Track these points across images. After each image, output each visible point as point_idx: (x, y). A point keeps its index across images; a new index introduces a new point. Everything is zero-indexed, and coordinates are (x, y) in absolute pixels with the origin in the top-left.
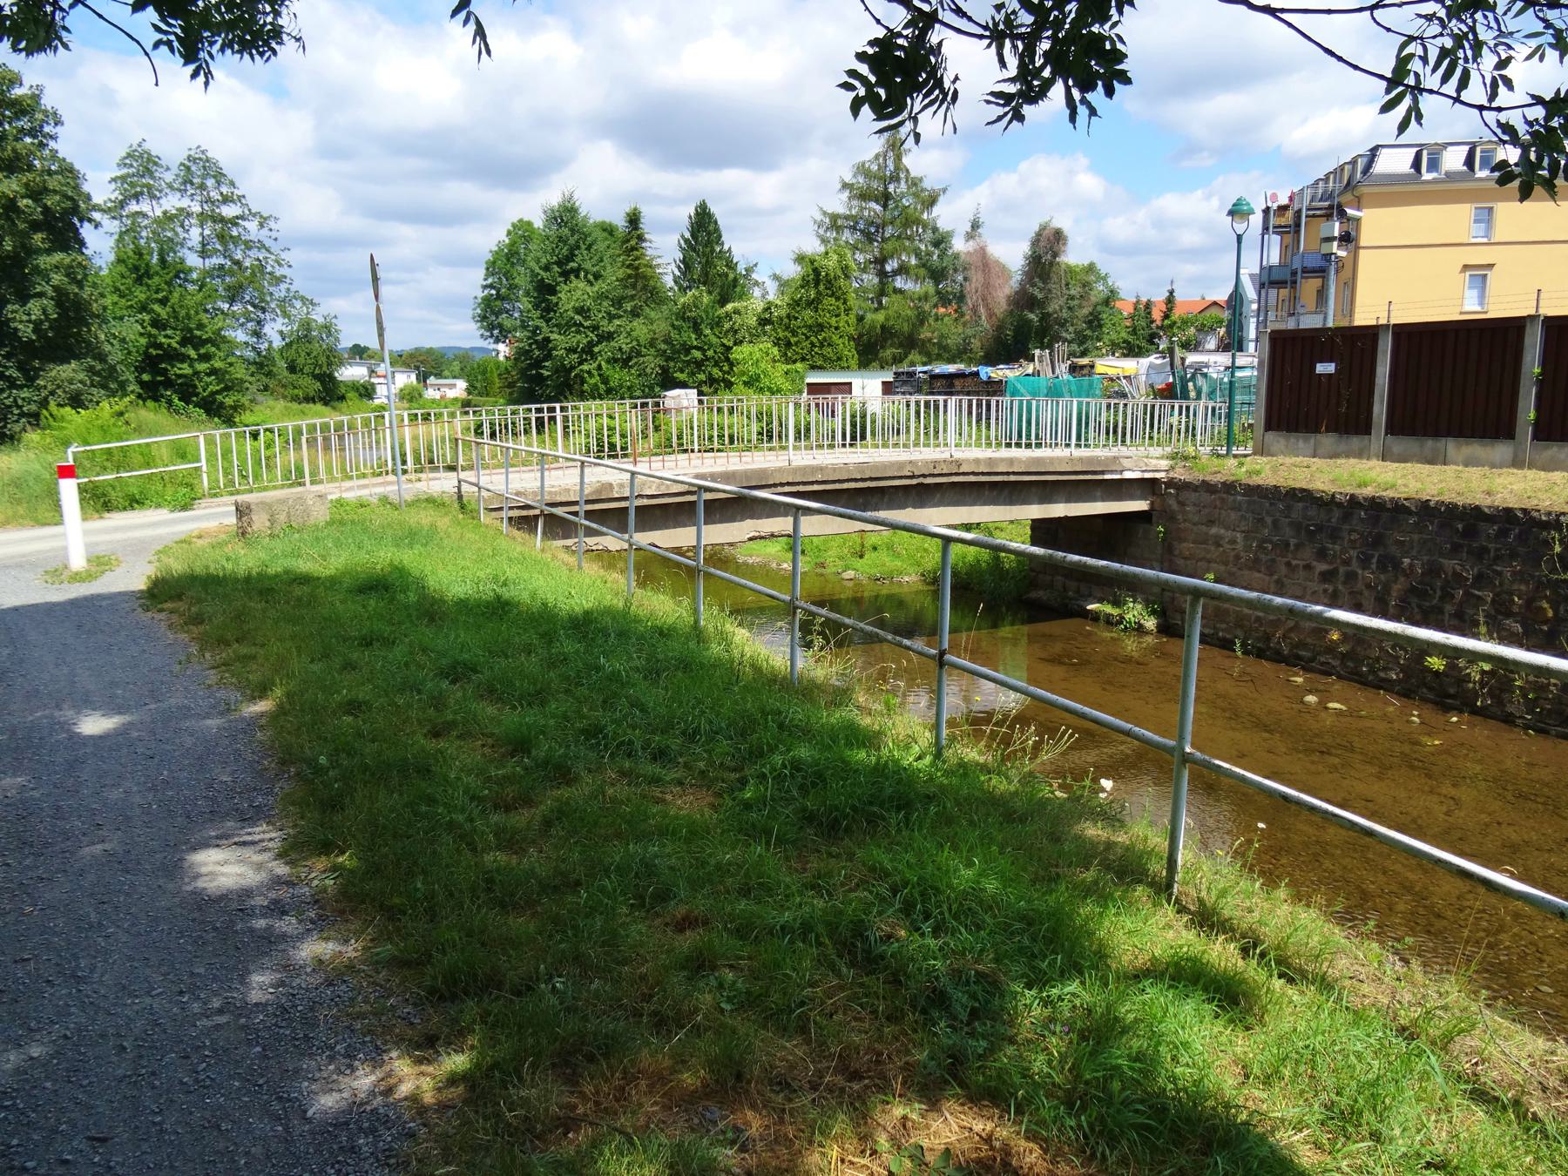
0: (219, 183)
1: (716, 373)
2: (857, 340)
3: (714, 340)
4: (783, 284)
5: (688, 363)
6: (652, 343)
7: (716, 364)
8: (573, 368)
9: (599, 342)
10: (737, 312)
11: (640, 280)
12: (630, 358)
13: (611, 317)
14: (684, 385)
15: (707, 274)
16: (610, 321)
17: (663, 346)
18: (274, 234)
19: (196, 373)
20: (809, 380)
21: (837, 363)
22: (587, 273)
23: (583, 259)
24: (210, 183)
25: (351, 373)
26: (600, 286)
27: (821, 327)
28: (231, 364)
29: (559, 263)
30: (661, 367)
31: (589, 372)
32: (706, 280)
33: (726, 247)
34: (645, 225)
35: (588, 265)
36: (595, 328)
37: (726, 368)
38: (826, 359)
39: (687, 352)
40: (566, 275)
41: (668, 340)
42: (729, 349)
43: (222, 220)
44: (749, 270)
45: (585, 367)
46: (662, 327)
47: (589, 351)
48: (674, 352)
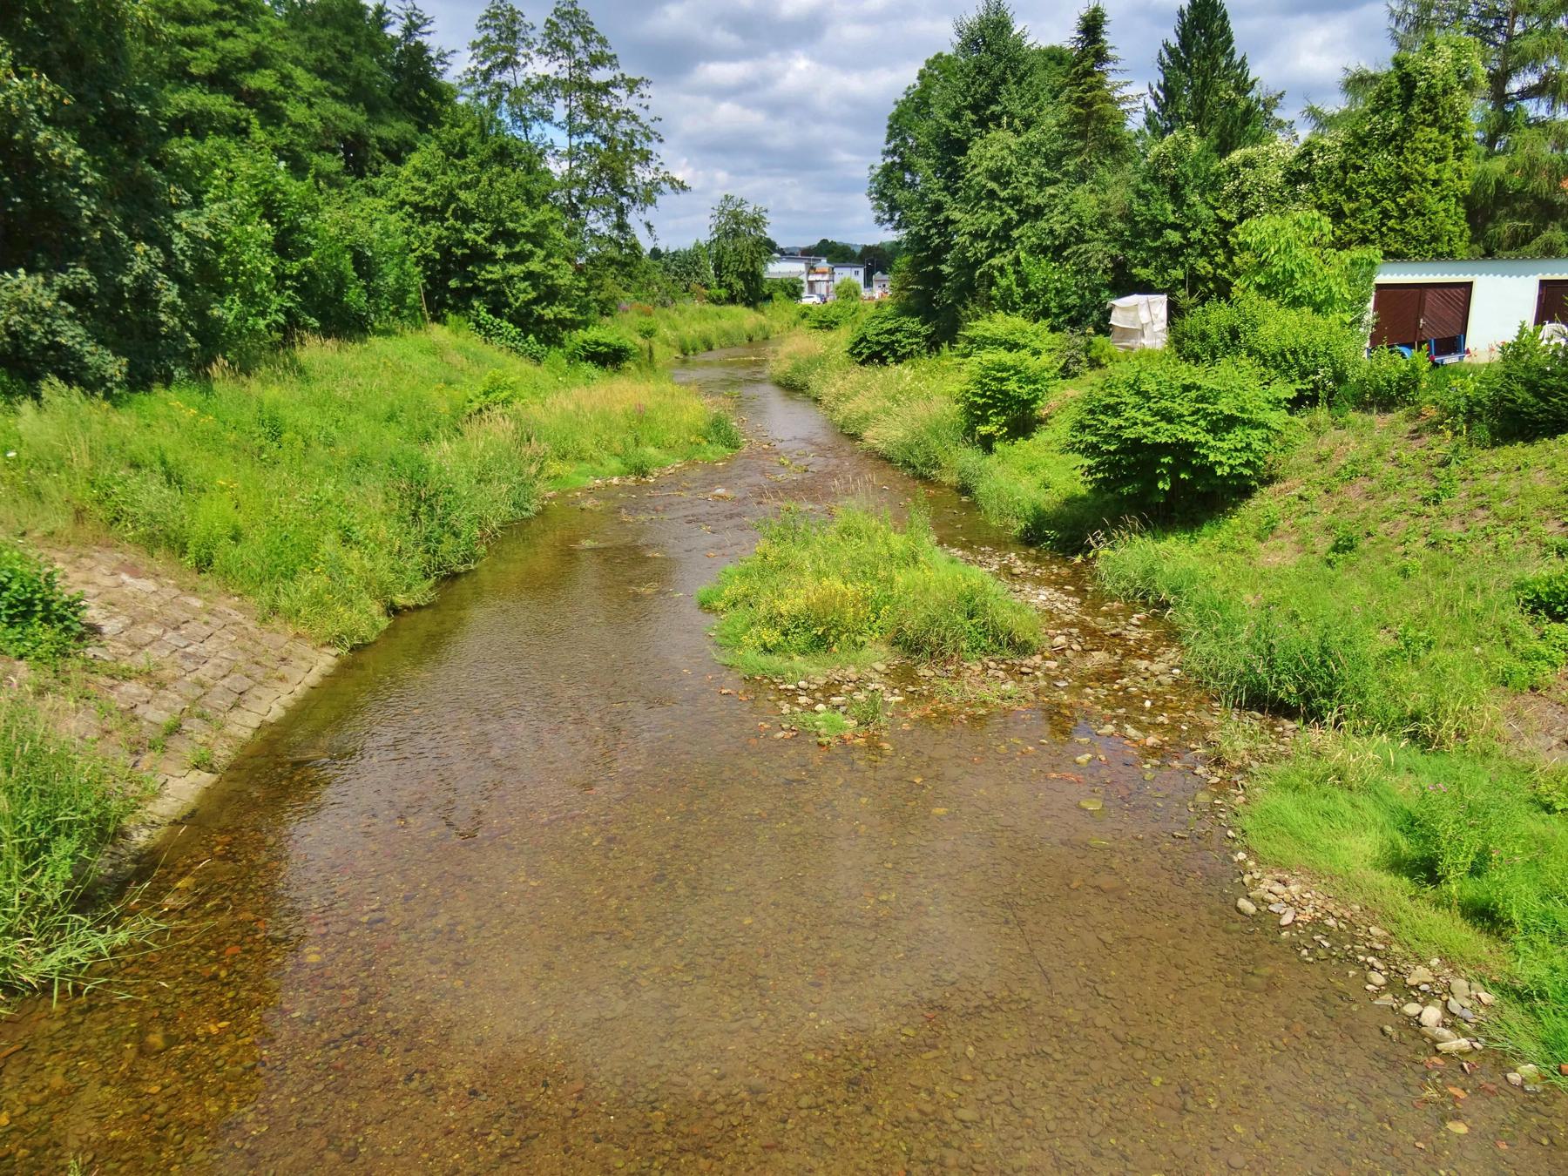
0: (587, 41)
1: (1203, 267)
2: (1467, 201)
3: (1204, 212)
4: (1324, 122)
5: (1156, 252)
6: (1102, 221)
7: (1204, 252)
8: (979, 262)
9: (1021, 222)
10: (1249, 163)
11: (1093, 125)
12: (1065, 246)
13: (1043, 182)
14: (1146, 288)
15: (1201, 105)
16: (1040, 187)
17: (1119, 225)
18: (645, 102)
19: (509, 279)
20: (1381, 279)
21: (1432, 247)
22: (1012, 116)
23: (1011, 100)
24: (577, 41)
25: (777, 269)
26: (1033, 135)
27: (1406, 181)
28: (556, 267)
29: (975, 108)
30: (1113, 258)
31: (1001, 270)
32: (1200, 116)
33: (1237, 58)
34: (1111, 37)
35: (1015, 107)
36: (1016, 200)
37: (1221, 259)
38: (1407, 238)
39: (1158, 233)
40: (982, 123)
41: (1127, 217)
42: (1228, 226)
43: (589, 87)
44: (1269, 105)
45: (995, 261)
46: (1119, 196)
47: (1003, 237)
48: (1138, 234)
